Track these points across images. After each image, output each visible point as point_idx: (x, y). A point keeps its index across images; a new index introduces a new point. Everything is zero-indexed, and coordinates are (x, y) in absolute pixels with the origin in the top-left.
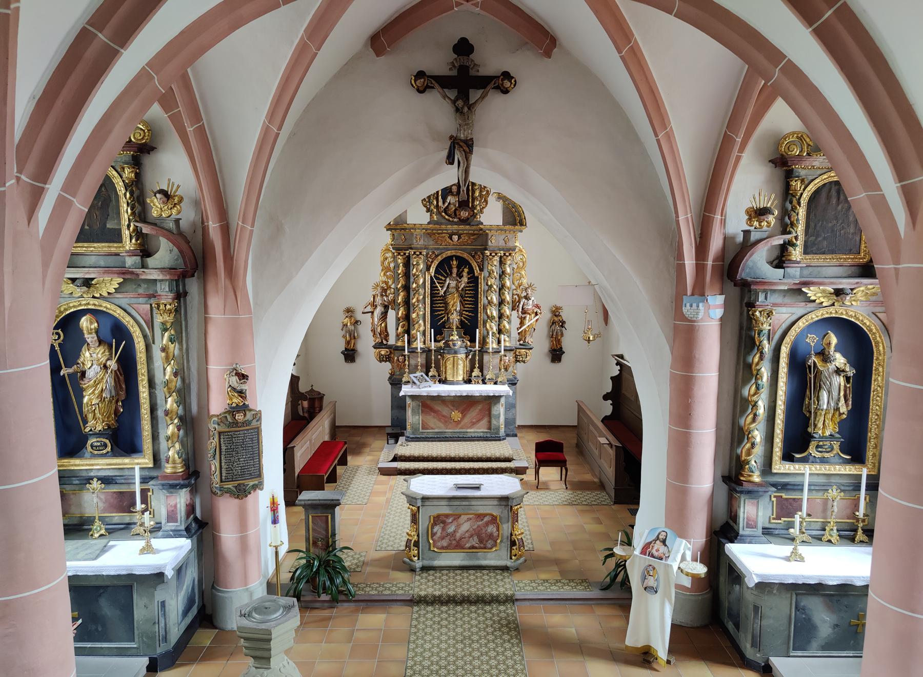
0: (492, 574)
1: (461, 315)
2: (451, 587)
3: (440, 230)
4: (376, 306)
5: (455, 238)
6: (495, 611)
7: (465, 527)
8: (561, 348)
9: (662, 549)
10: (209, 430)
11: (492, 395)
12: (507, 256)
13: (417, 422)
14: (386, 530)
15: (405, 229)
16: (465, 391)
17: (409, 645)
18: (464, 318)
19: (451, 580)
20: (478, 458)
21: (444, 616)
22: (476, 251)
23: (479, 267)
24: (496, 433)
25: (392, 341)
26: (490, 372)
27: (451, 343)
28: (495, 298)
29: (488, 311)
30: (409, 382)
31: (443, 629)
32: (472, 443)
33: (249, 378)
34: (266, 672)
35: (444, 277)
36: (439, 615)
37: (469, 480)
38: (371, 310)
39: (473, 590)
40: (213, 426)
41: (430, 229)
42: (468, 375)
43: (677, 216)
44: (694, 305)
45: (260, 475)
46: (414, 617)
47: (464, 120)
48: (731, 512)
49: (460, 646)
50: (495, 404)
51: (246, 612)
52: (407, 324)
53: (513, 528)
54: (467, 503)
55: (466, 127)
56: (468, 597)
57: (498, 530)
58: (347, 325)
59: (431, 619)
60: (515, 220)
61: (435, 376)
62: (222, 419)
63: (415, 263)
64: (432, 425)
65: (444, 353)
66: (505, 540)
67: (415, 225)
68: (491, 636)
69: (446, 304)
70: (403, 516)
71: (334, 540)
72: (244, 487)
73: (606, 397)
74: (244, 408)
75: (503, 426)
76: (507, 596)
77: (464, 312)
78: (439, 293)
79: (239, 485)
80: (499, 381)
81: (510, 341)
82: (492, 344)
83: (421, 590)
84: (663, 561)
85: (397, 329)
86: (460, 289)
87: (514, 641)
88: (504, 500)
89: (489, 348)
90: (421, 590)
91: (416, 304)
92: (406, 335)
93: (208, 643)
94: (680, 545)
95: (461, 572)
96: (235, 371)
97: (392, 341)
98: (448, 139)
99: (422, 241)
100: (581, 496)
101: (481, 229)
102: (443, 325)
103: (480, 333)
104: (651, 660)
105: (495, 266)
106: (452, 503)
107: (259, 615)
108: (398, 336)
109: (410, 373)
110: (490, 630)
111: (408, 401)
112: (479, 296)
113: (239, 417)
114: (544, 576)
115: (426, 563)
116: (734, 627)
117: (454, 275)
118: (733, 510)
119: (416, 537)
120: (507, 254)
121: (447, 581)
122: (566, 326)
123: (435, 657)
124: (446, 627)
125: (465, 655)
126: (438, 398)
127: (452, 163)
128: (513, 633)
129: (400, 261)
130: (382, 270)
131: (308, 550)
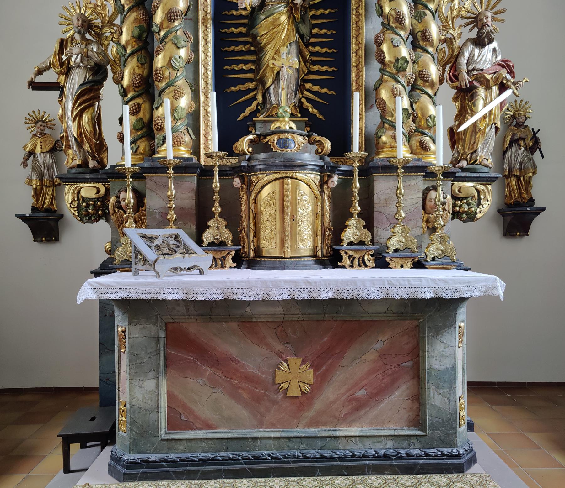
11: (429, 295)
18: (309, 100)
26: (398, 229)
50: (438, 331)
61: (222, 243)
77: (308, 86)
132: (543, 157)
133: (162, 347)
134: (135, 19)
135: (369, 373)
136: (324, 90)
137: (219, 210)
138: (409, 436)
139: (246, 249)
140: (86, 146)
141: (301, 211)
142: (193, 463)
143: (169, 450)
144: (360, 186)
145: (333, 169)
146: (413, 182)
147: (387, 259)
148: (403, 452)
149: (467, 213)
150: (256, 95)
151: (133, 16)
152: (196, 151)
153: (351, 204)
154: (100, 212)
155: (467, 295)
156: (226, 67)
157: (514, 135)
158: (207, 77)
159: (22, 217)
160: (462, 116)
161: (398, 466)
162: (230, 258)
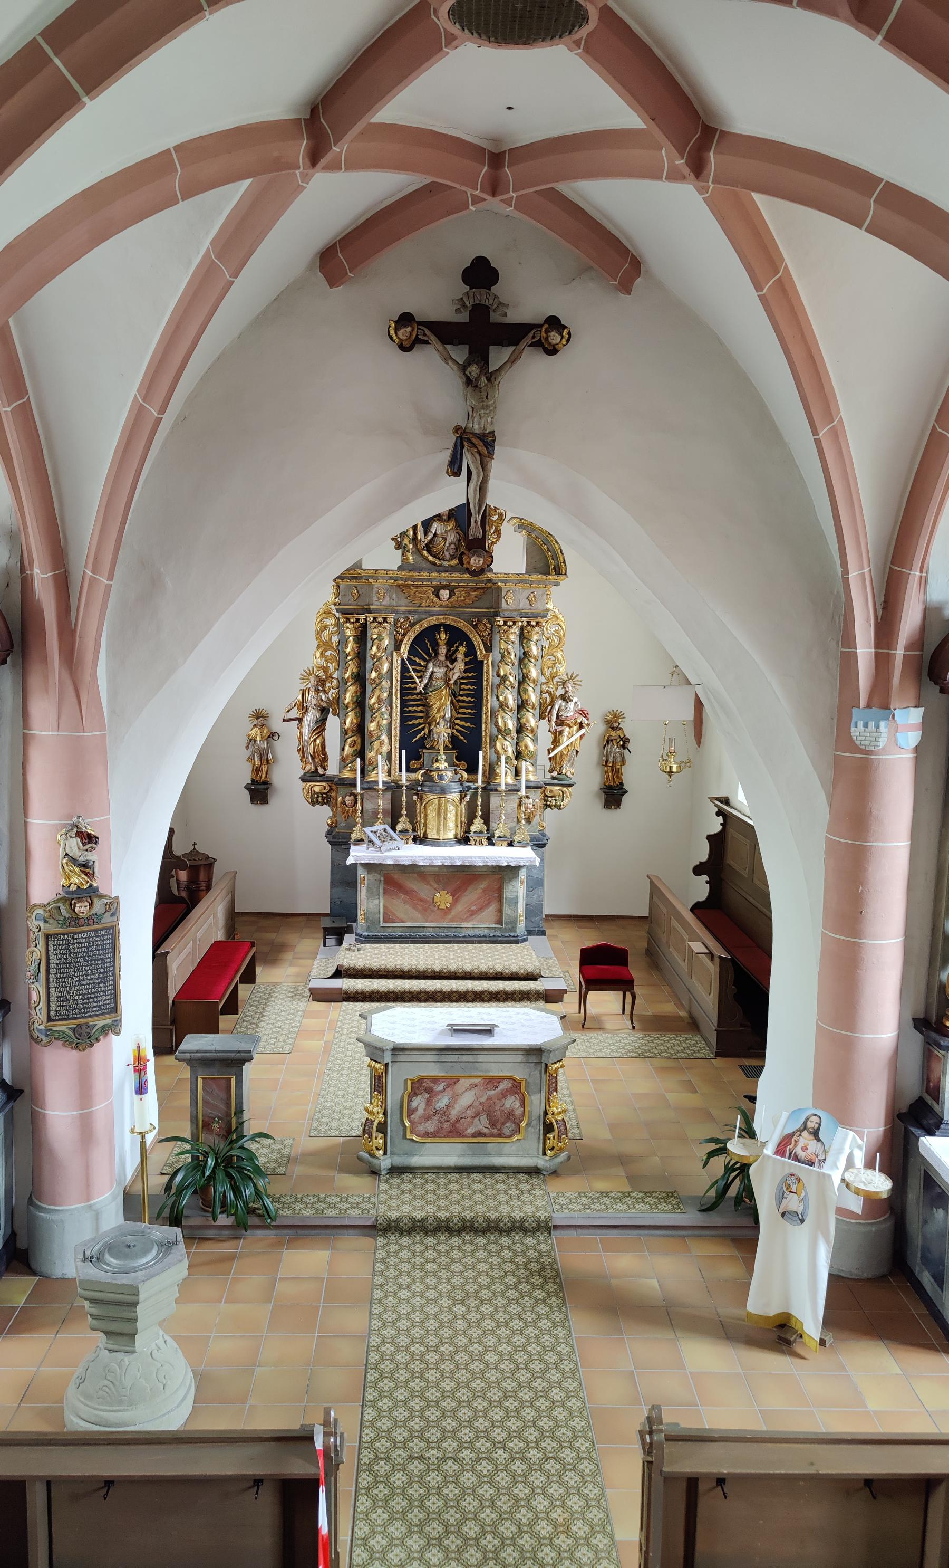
0: (512, 1181)
1: (452, 725)
2: (443, 1203)
3: (419, 580)
4: (307, 709)
5: (445, 594)
6: (518, 1247)
7: (467, 1099)
8: (622, 784)
9: (813, 1146)
10: (28, 930)
11: (505, 864)
12: (533, 626)
13: (377, 910)
14: (326, 1100)
15: (358, 578)
16: (459, 857)
17: (371, 1307)
18: (458, 731)
19: (442, 1192)
20: (481, 973)
21: (431, 1254)
24: (511, 932)
25: (333, 768)
26: (501, 825)
27: (435, 774)
28: (511, 699)
29: (500, 720)
30: (362, 840)
31: (430, 1278)
32: (470, 946)
33: (100, 842)
34: (127, 1359)
35: (425, 660)
36: (422, 1252)
37: (471, 1017)
38: (297, 716)
39: (480, 1209)
40: (36, 923)
41: (401, 579)
42: (464, 829)
43: (846, 571)
44: (871, 724)
45: (115, 1009)
46: (379, 1256)
47: (481, 400)
48: (928, 1081)
49: (459, 1309)
50: (510, 880)
51: (94, 1253)
52: (359, 741)
53: (549, 1102)
54: (470, 1058)
55: (483, 411)
56: (472, 1221)
57: (523, 1105)
58: (255, 740)
59: (408, 1261)
60: (548, 565)
61: (407, 831)
62: (52, 912)
63: (375, 637)
64: (401, 915)
65: (422, 791)
67: (376, 571)
68: (513, 1292)
69: (427, 707)
70: (354, 1075)
71: (241, 1120)
72: (88, 1030)
73: (698, 870)
74: (90, 894)
75: (523, 918)
76: (538, 1221)
77: (457, 722)
78: (415, 689)
79: (79, 1026)
80: (516, 840)
82: (505, 778)
83: (390, 1208)
84: (815, 1169)
85: (343, 749)
86: (452, 682)
87: (554, 1301)
88: (535, 1054)
89: (500, 784)
90: (390, 1208)
91: (376, 706)
92: (358, 760)
93: (21, 1301)
94: (844, 1139)
95: (458, 1176)
96: (75, 830)
97: (333, 768)
98: (452, 431)
99: (388, 599)
100: (661, 1047)
101: (490, 580)
102: (422, 743)
103: (484, 757)
104: (792, 1339)
105: (513, 643)
106: (443, 1058)
107: (116, 1258)
109: (363, 825)
110: (510, 1280)
111: (361, 874)
113: (82, 908)
114: (601, 1185)
115: (399, 1161)
116: (932, 1280)
117: (442, 658)
118: (934, 1077)
119: (381, 1116)
120: (533, 623)
121: (434, 1192)
122: (630, 746)
123: (417, 1329)
124: (435, 1274)
125: (470, 1327)
126: (413, 870)
127: (457, 474)
128: (551, 1287)
129: (349, 631)
130: (318, 647)
131: (195, 1137)
135: (478, 899)
141: (449, 815)
142: (395, 937)
146: (512, 797)
148: (492, 935)
149: (555, 806)
153: (476, 811)
155: (522, 864)
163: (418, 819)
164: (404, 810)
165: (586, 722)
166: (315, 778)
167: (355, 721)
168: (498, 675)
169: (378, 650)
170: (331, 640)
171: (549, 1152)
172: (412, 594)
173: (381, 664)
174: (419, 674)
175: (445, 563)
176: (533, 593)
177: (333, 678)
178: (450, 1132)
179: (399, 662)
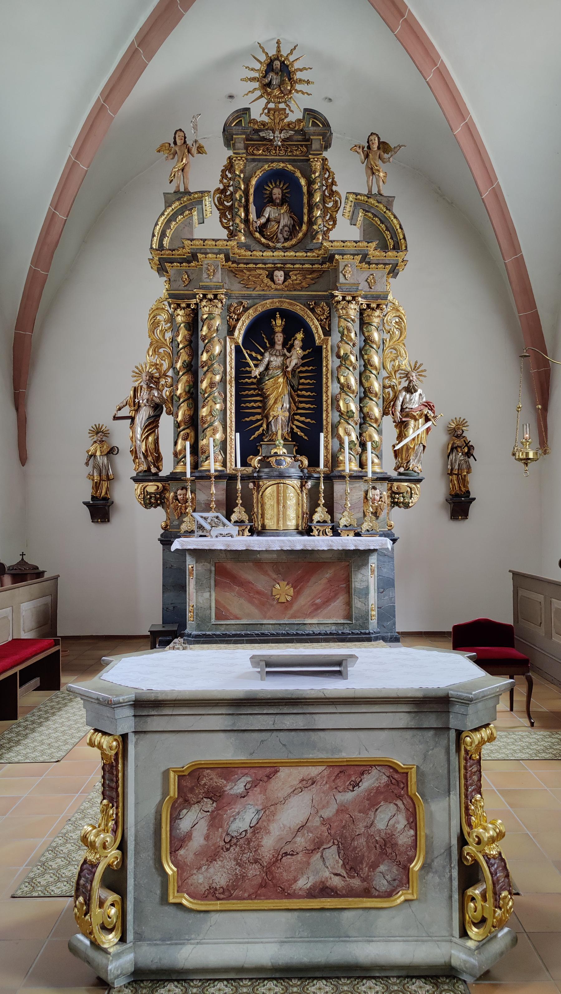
4: (139, 406)
5: (279, 275)
8: (468, 492)
11: (352, 548)
12: (373, 309)
18: (298, 427)
22: (317, 300)
23: (323, 328)
25: (167, 469)
26: (346, 513)
27: (273, 460)
29: (341, 403)
52: (192, 434)
53: (468, 815)
57: (413, 823)
61: (242, 522)
63: (205, 317)
64: (234, 609)
66: (438, 863)
67: (204, 240)
69: (265, 398)
77: (297, 417)
78: (250, 372)
81: (381, 465)
91: (209, 390)
105: (353, 320)
106: (244, 722)
108: (178, 457)
111: (190, 563)
112: (324, 380)
117: (279, 347)
119: (113, 854)
130: (151, 344)
132: (476, 460)
133: (213, 575)
134: (187, 381)
136: (308, 420)
137: (241, 502)
138: (344, 624)
139: (256, 525)
140: (150, 459)
141: (288, 503)
142: (229, 636)
143: (217, 630)
144: (324, 488)
145: (310, 477)
146: (357, 485)
147: (339, 531)
149: (403, 503)
150: (262, 423)
151: (184, 378)
152: (224, 464)
153: (319, 499)
154: (159, 502)
156: (242, 405)
157: (454, 443)
158: (231, 417)
159: (85, 503)
160: (401, 437)
161: (336, 638)
162: (247, 530)
163: (255, 510)
164: (239, 498)
165: (432, 415)
166: (147, 478)
167: (189, 413)
168: (338, 356)
169: (209, 329)
170: (164, 336)
171: (473, 931)
172: (245, 278)
173: (212, 345)
174: (255, 362)
175: (279, 245)
176: (372, 275)
177: (167, 376)
178: (261, 886)
179: (233, 347)
